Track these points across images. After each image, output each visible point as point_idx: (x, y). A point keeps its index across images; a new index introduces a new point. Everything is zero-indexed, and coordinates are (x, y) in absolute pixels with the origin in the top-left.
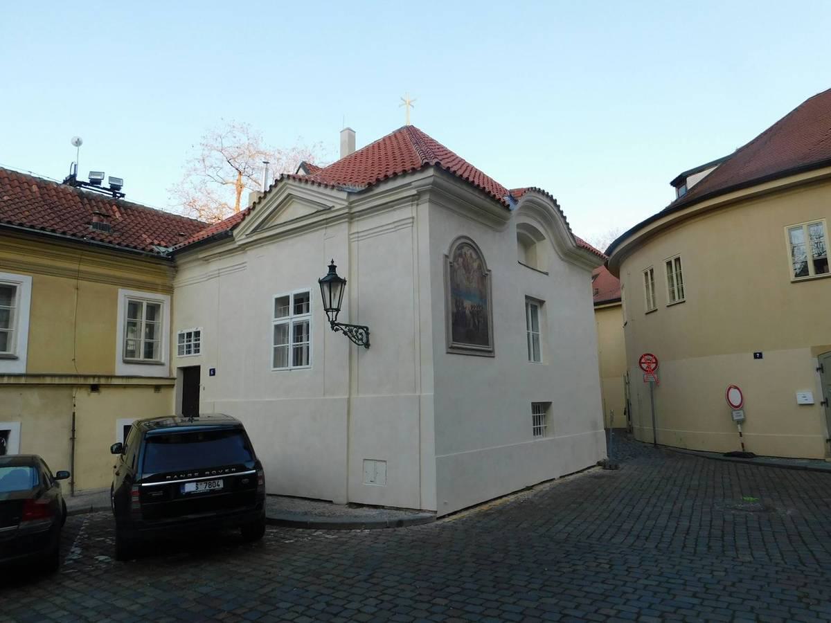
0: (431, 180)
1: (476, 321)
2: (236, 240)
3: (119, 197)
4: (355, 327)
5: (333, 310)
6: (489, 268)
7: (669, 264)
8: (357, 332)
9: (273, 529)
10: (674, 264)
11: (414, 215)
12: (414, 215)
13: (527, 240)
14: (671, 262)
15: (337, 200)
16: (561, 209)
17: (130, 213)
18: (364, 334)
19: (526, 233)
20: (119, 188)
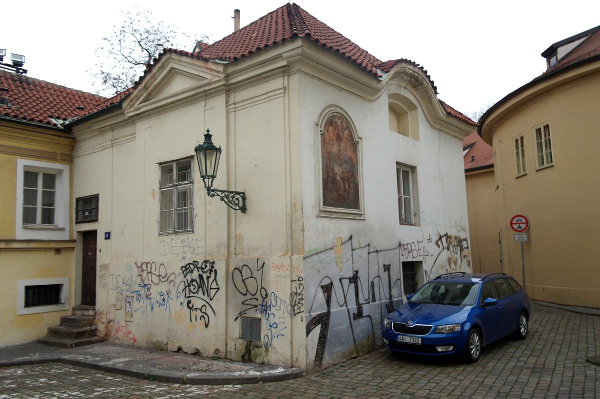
0: (300, 50)
1: (347, 186)
3: (22, 73)
4: (232, 192)
6: (360, 136)
7: (538, 131)
8: (233, 197)
9: (151, 384)
10: (543, 132)
11: (286, 84)
12: (286, 84)
13: (398, 112)
14: (540, 129)
15: (212, 74)
16: (435, 85)
17: (26, 86)
18: (240, 199)
19: (396, 102)
20: (21, 64)
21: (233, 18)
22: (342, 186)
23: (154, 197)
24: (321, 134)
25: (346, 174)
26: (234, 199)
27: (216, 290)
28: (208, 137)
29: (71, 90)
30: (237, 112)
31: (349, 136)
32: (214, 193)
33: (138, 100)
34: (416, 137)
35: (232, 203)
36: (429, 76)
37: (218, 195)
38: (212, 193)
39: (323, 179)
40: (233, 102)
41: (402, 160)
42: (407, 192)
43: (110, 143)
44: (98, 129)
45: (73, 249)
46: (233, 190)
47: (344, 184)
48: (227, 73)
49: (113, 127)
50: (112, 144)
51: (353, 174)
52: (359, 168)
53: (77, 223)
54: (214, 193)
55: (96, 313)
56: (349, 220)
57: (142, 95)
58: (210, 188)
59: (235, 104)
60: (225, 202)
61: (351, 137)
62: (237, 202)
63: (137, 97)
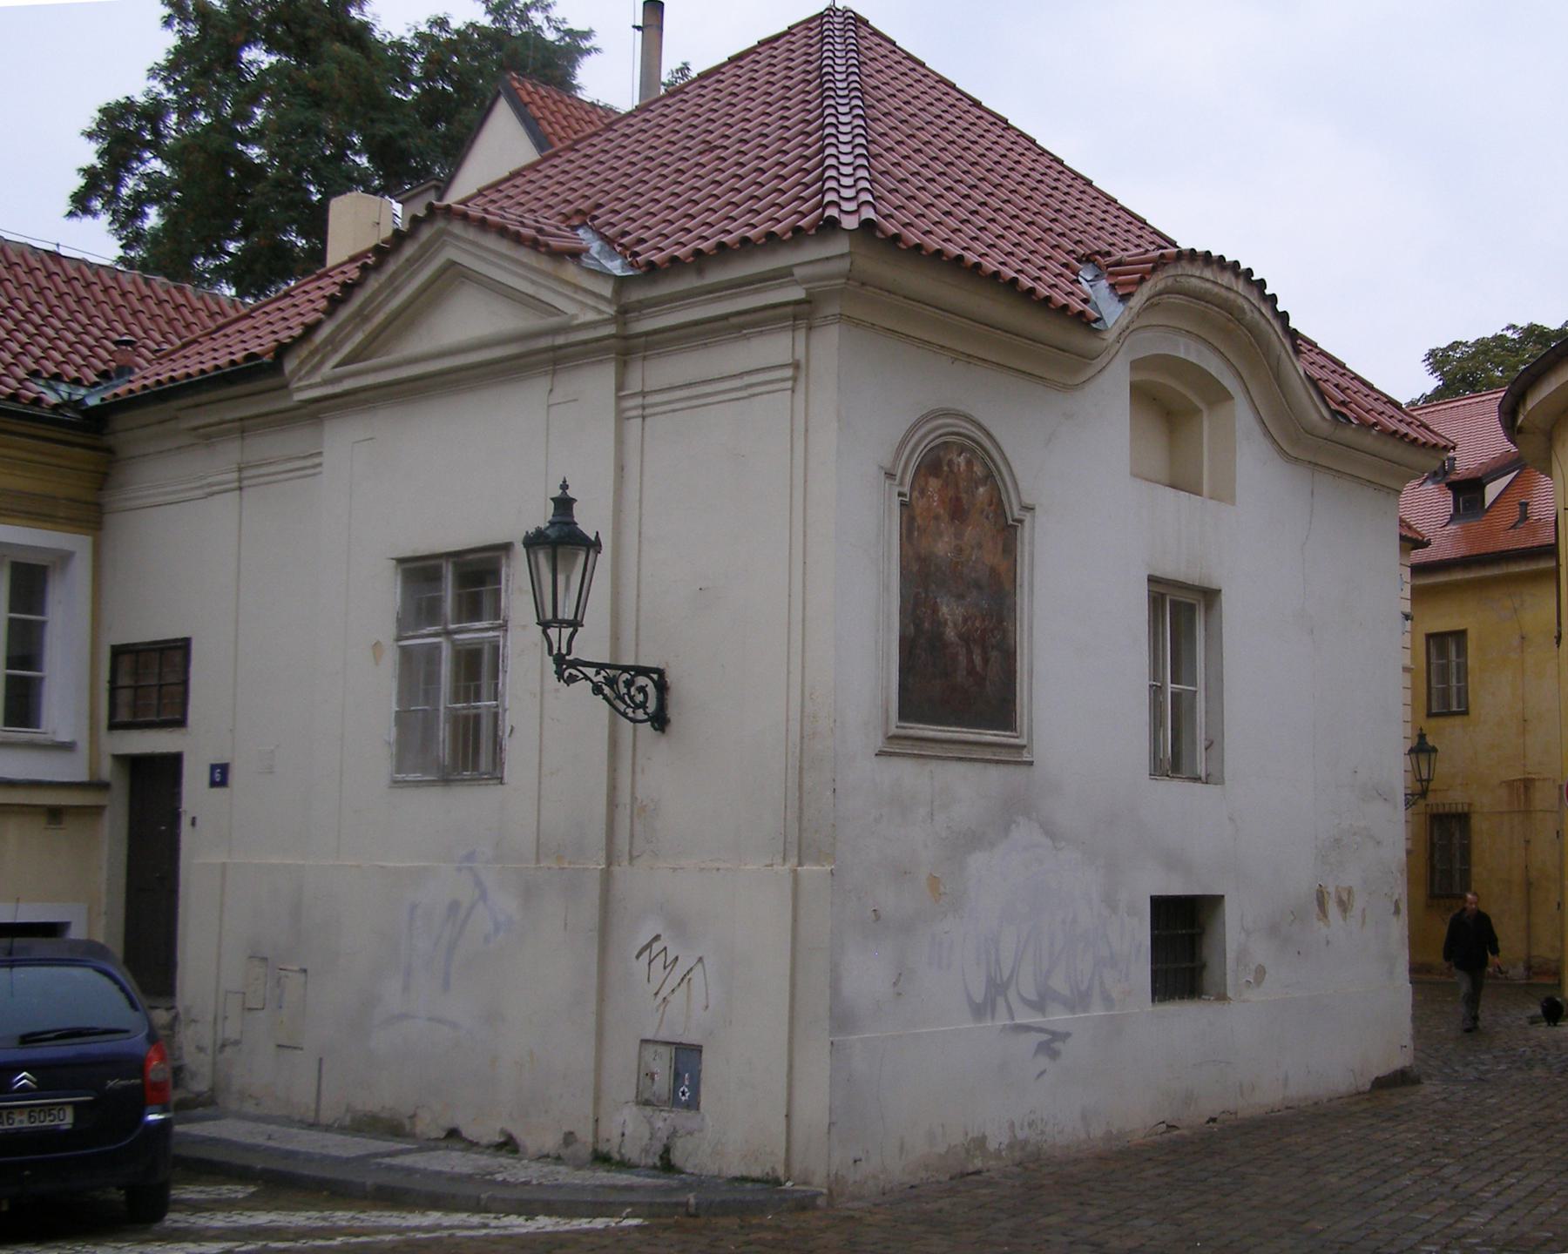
0: (844, 265)
1: (978, 660)
2: (294, 385)
4: (626, 669)
5: (562, 623)
6: (1027, 500)
8: (629, 684)
11: (800, 354)
12: (800, 354)
18: (651, 690)
21: (638, 28)
22: (961, 658)
23: (377, 658)
24: (902, 504)
25: (977, 624)
26: (633, 691)
27: (663, 953)
28: (564, 504)
29: (81, 263)
30: (648, 421)
31: (990, 505)
32: (574, 672)
33: (335, 350)
34: (1225, 494)
35: (625, 703)
36: (1274, 298)
37: (587, 678)
38: (570, 670)
39: (902, 639)
40: (638, 389)
41: (1172, 569)
42: (1181, 666)
43: (235, 475)
44: (195, 429)
45: (97, 810)
46: (628, 660)
47: (970, 652)
48: (624, 300)
49: (244, 428)
50: (240, 480)
51: (1001, 621)
52: (1018, 602)
53: (113, 726)
54: (574, 672)
55: (176, 1018)
56: (979, 765)
57: (349, 337)
58: (564, 656)
59: (644, 394)
60: (606, 698)
61: (997, 504)
62: (640, 697)
63: (333, 343)
